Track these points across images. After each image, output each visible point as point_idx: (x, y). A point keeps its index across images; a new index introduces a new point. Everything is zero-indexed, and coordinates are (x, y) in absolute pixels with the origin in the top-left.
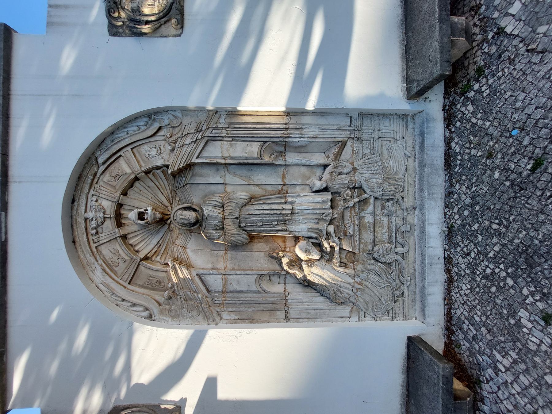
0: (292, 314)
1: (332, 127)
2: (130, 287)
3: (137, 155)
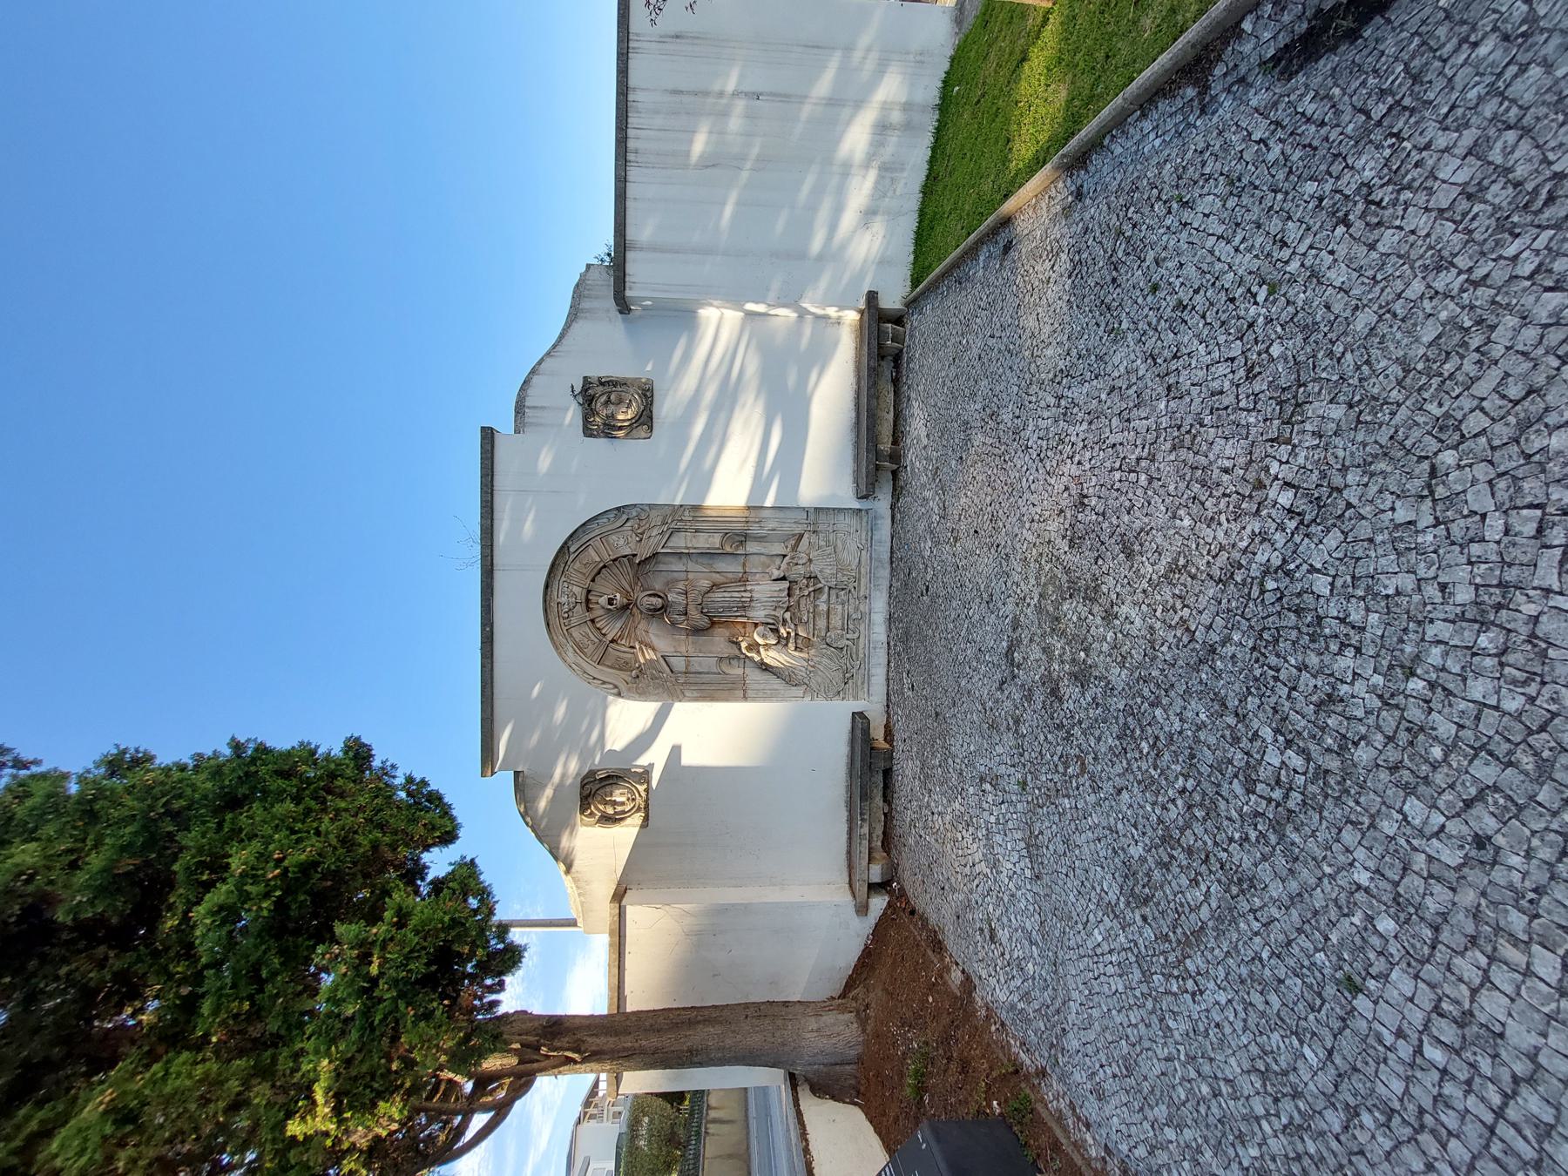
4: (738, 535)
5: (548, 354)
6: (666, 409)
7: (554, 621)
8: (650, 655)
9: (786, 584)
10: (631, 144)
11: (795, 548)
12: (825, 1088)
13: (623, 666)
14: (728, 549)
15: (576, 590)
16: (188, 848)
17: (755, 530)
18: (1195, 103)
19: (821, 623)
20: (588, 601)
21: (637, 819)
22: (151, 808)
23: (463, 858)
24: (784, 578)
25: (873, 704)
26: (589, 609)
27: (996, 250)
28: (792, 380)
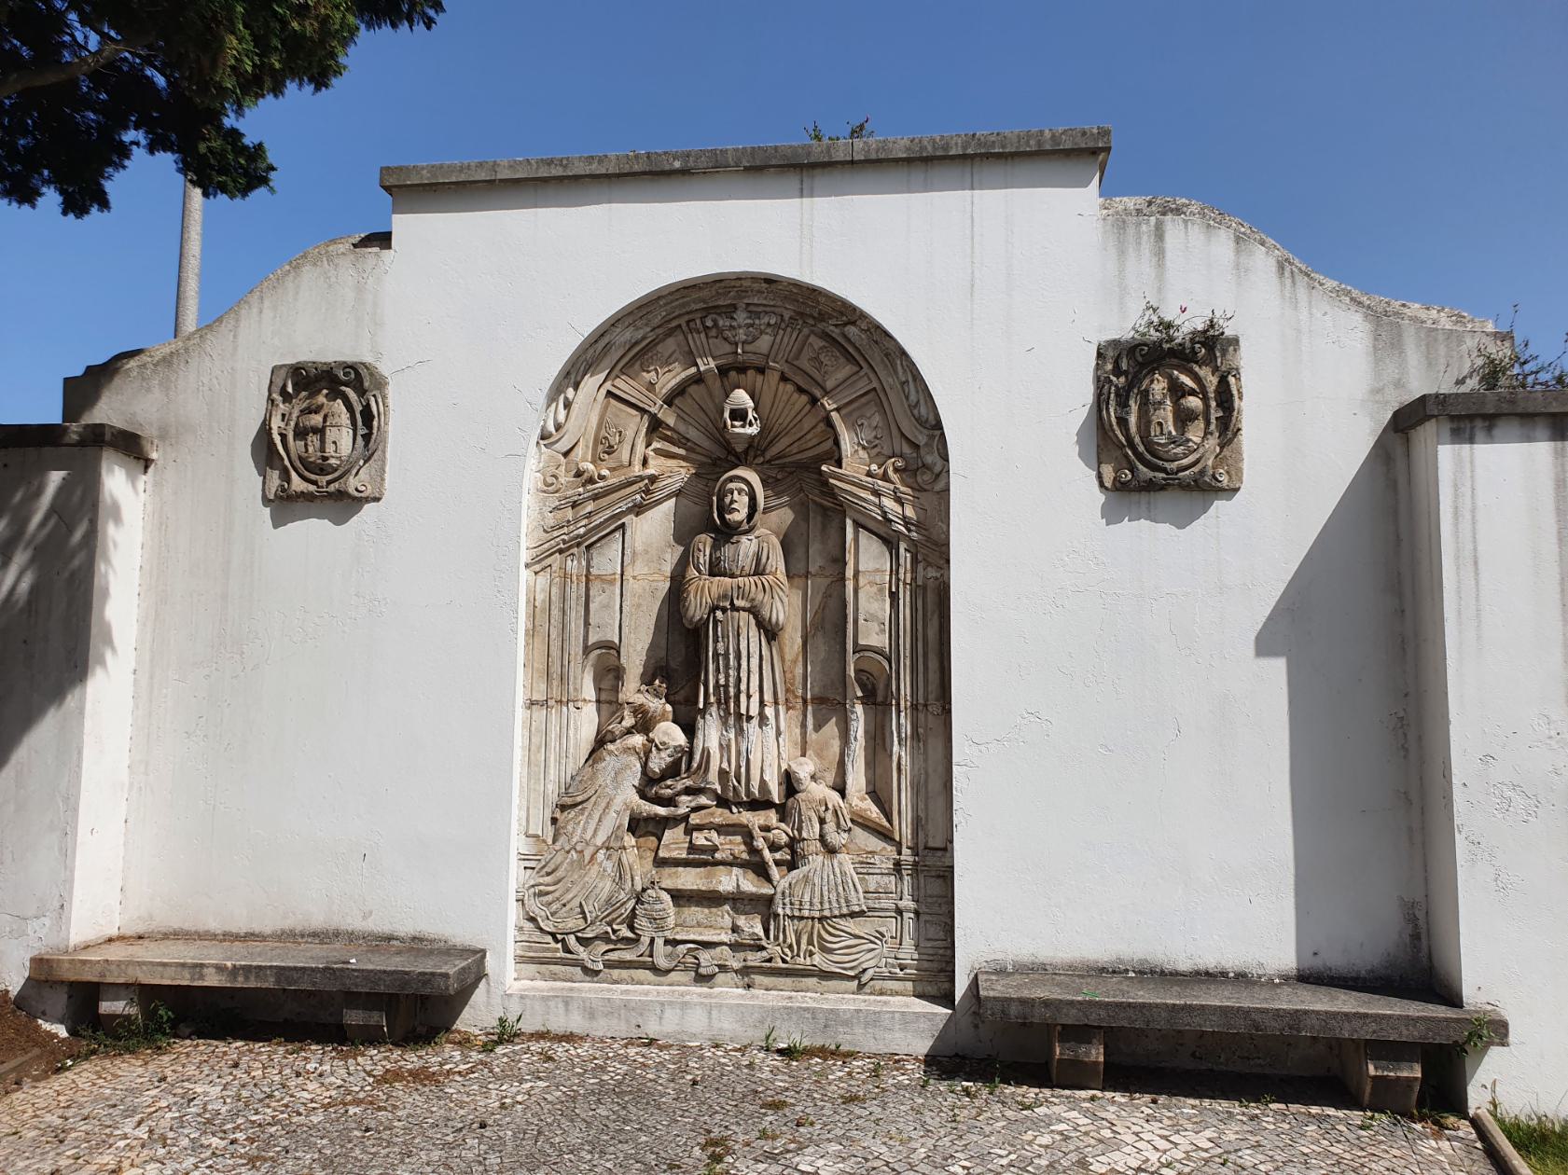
0: (540, 714)
1: (921, 806)
2: (603, 391)
3: (863, 400)
20: (742, 369)
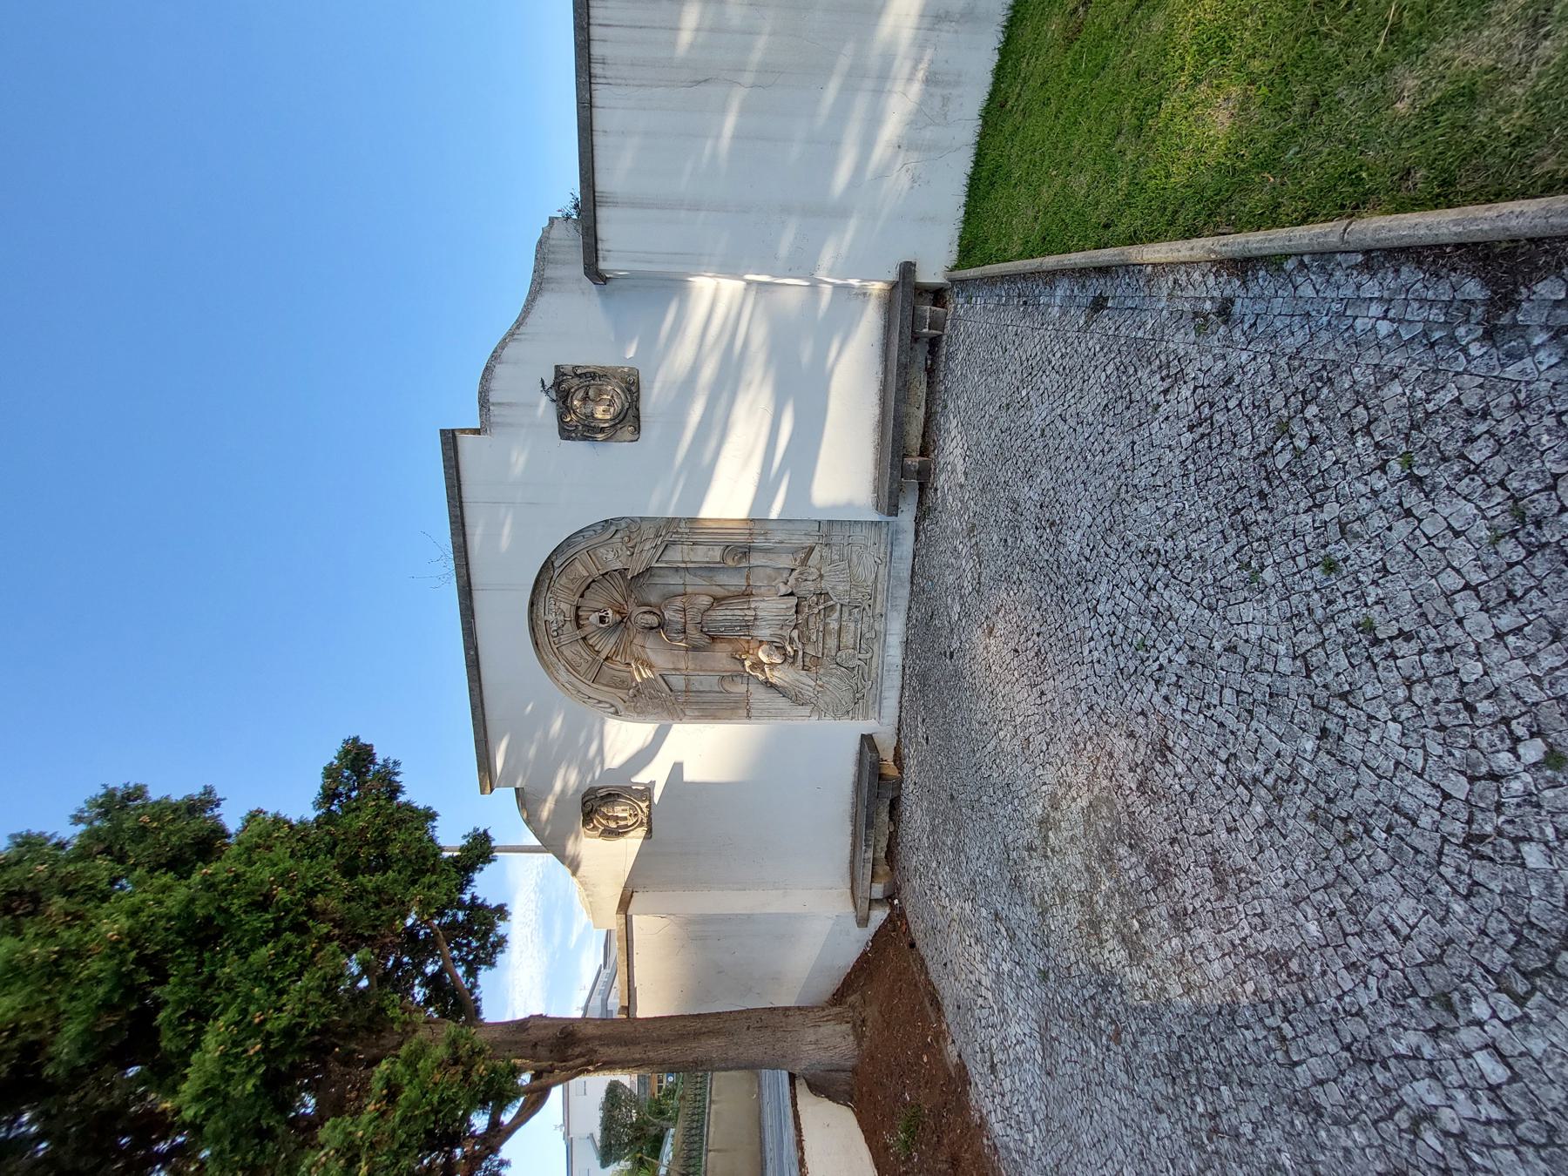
4: (741, 545)
5: (511, 334)
6: (652, 401)
7: (543, 639)
8: (647, 673)
9: (794, 601)
10: (597, 50)
11: (804, 562)
12: (820, 1087)
13: (622, 684)
14: (730, 562)
15: (564, 606)
16: (166, 1003)
17: (759, 542)
18: (1478, 312)
19: (832, 642)
20: (577, 617)
21: (641, 832)
22: (122, 963)
23: (476, 830)
24: (792, 594)
25: (882, 726)
26: (579, 626)
27: (1085, 298)
28: (806, 353)
